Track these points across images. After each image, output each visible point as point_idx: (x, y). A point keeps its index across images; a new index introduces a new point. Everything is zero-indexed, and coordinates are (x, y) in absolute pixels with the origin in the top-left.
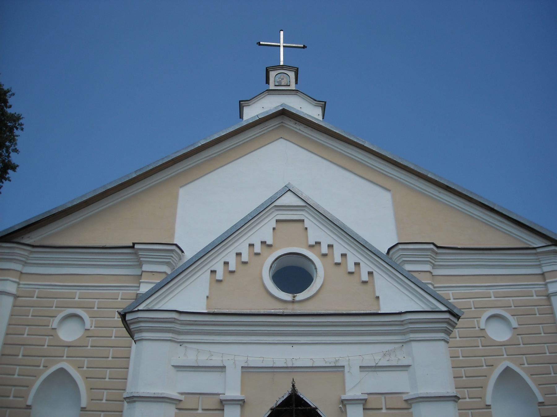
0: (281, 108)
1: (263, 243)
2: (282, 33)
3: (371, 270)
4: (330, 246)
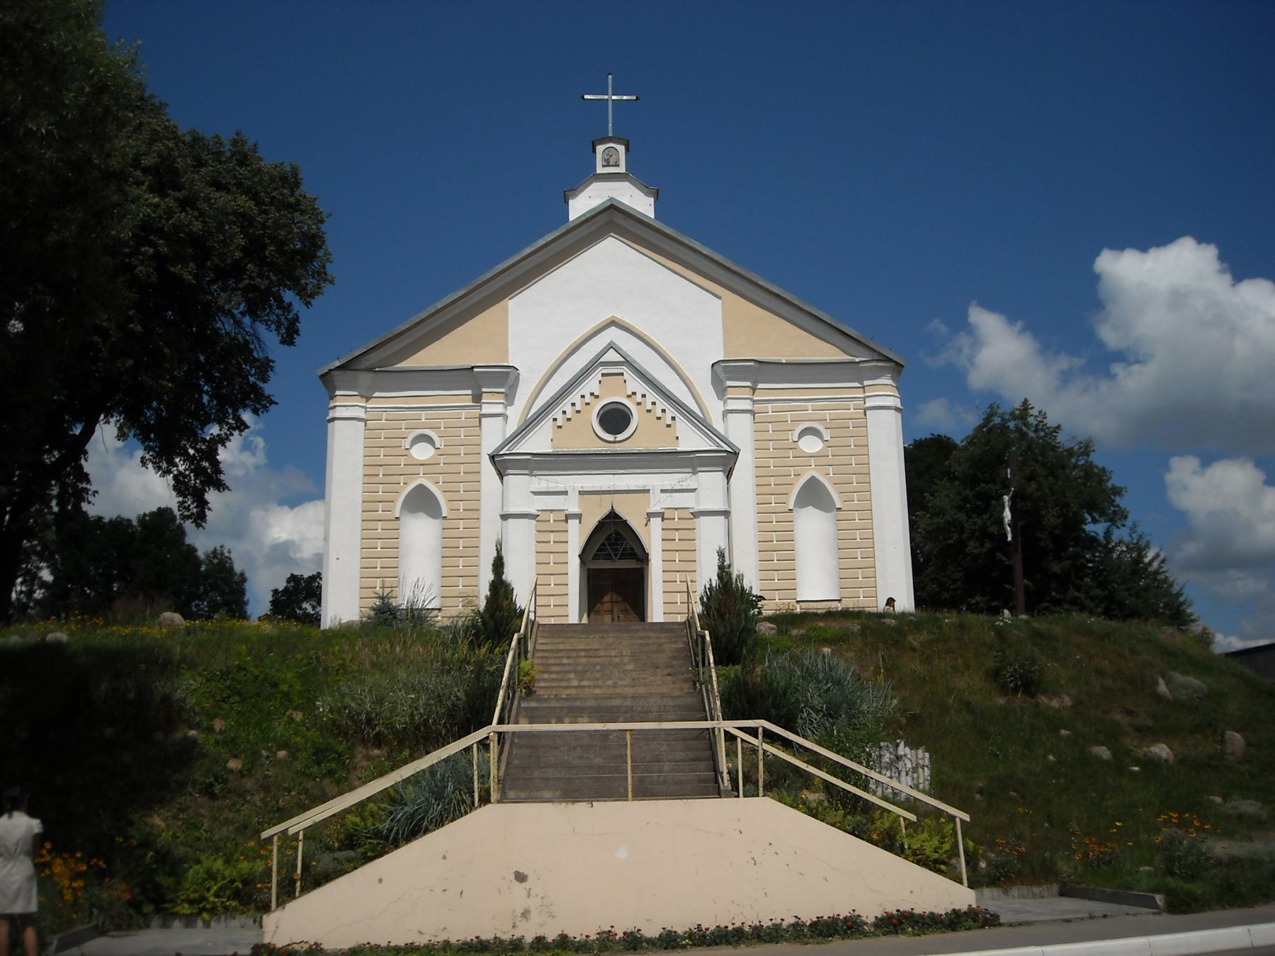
0: (609, 203)
1: (592, 394)
3: (674, 415)
4: (644, 396)
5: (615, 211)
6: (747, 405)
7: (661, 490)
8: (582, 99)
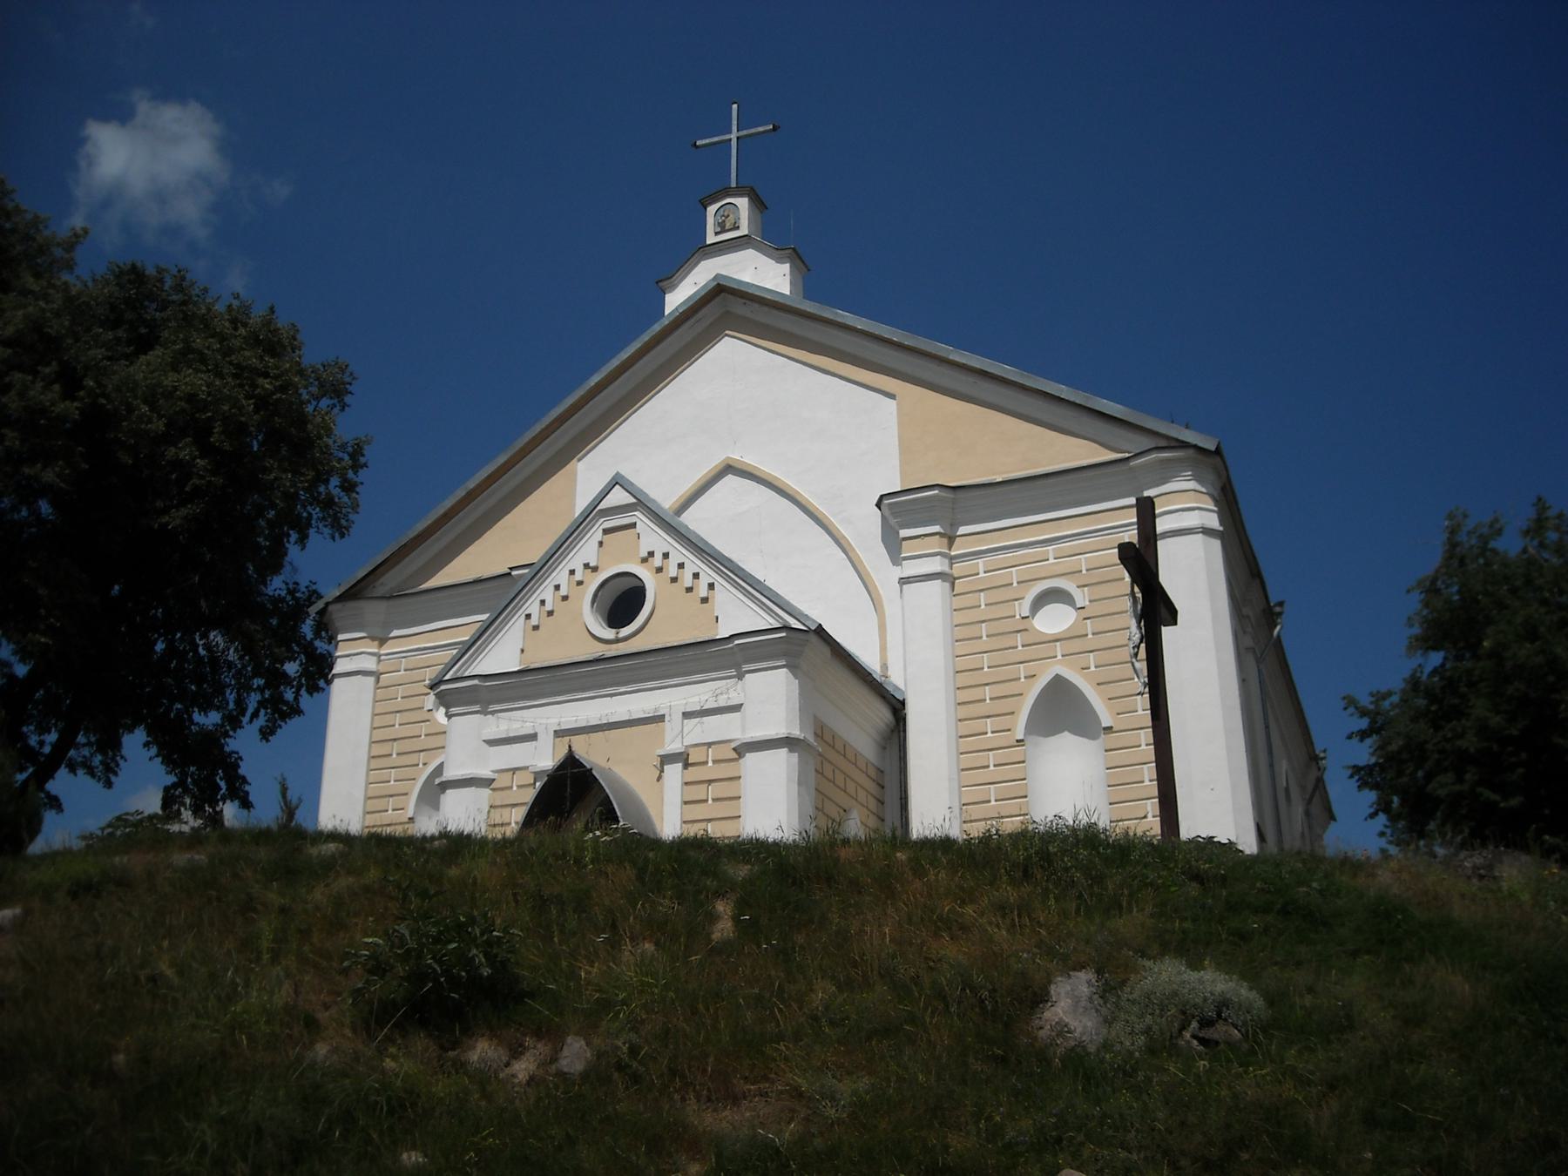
1: (586, 566)
2: (735, 106)
3: (711, 581)
4: (666, 556)
5: (730, 296)
6: (936, 565)
7: (684, 713)
8: (694, 148)
